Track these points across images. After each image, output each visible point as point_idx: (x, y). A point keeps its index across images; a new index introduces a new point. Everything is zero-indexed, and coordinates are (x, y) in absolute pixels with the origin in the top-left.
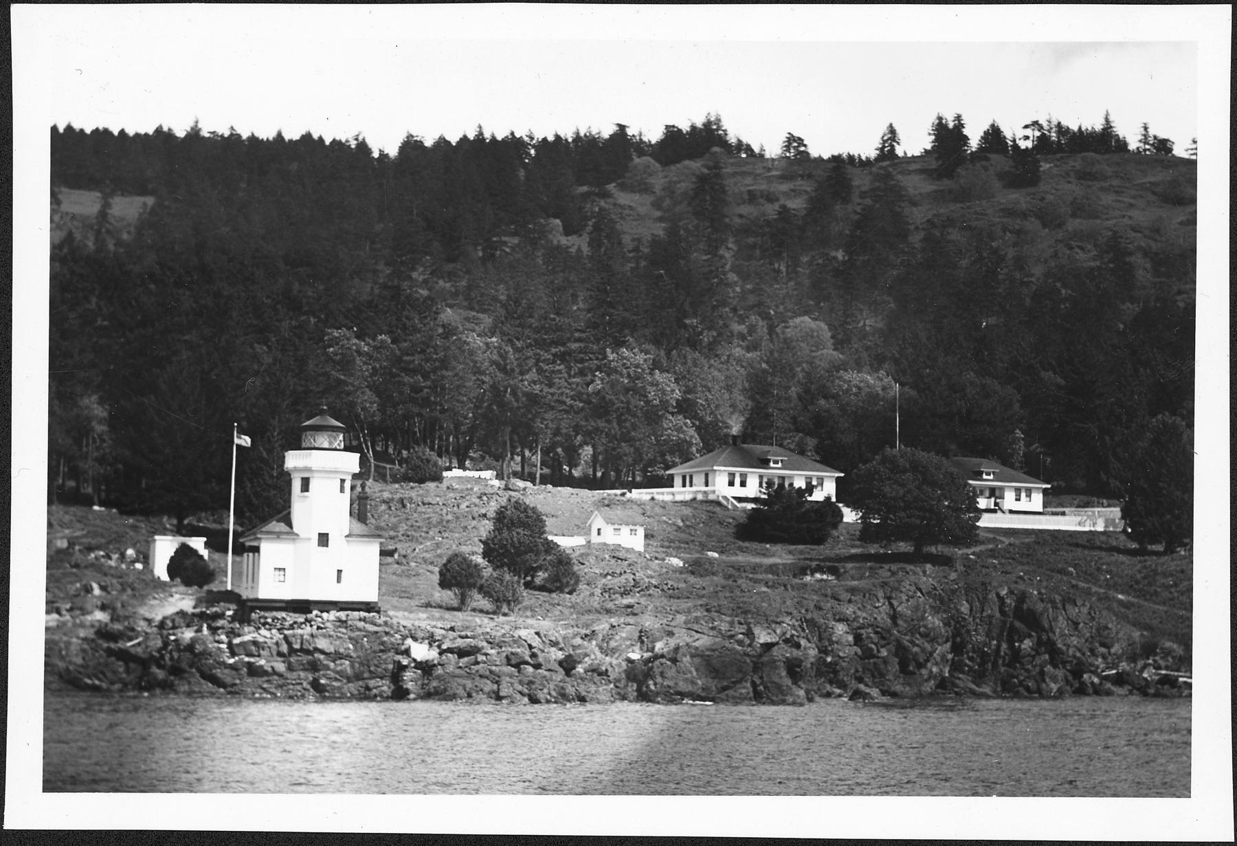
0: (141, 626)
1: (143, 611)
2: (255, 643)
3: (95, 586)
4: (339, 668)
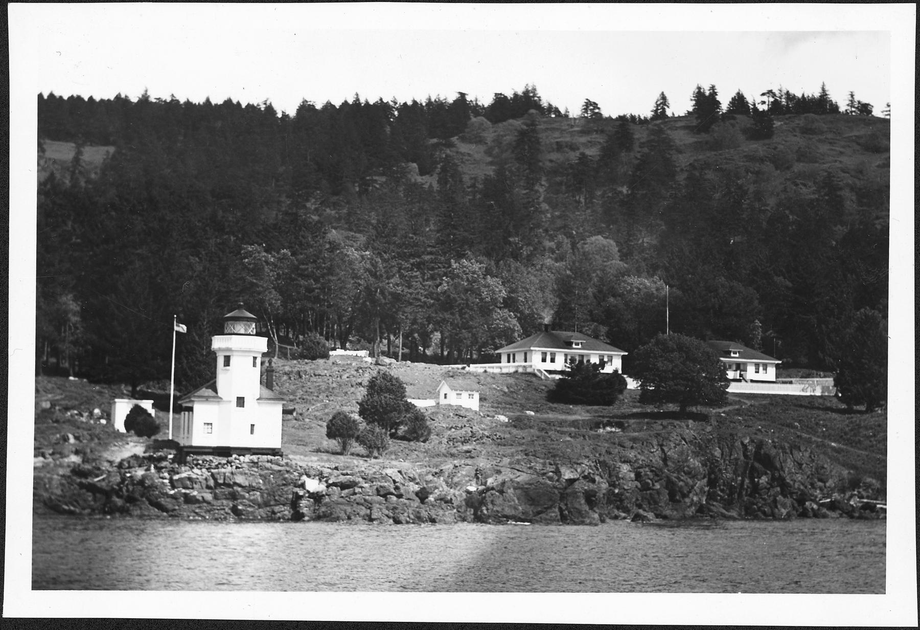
0: (105, 466)
1: (107, 455)
2: (190, 479)
3: (71, 436)
4: (252, 498)
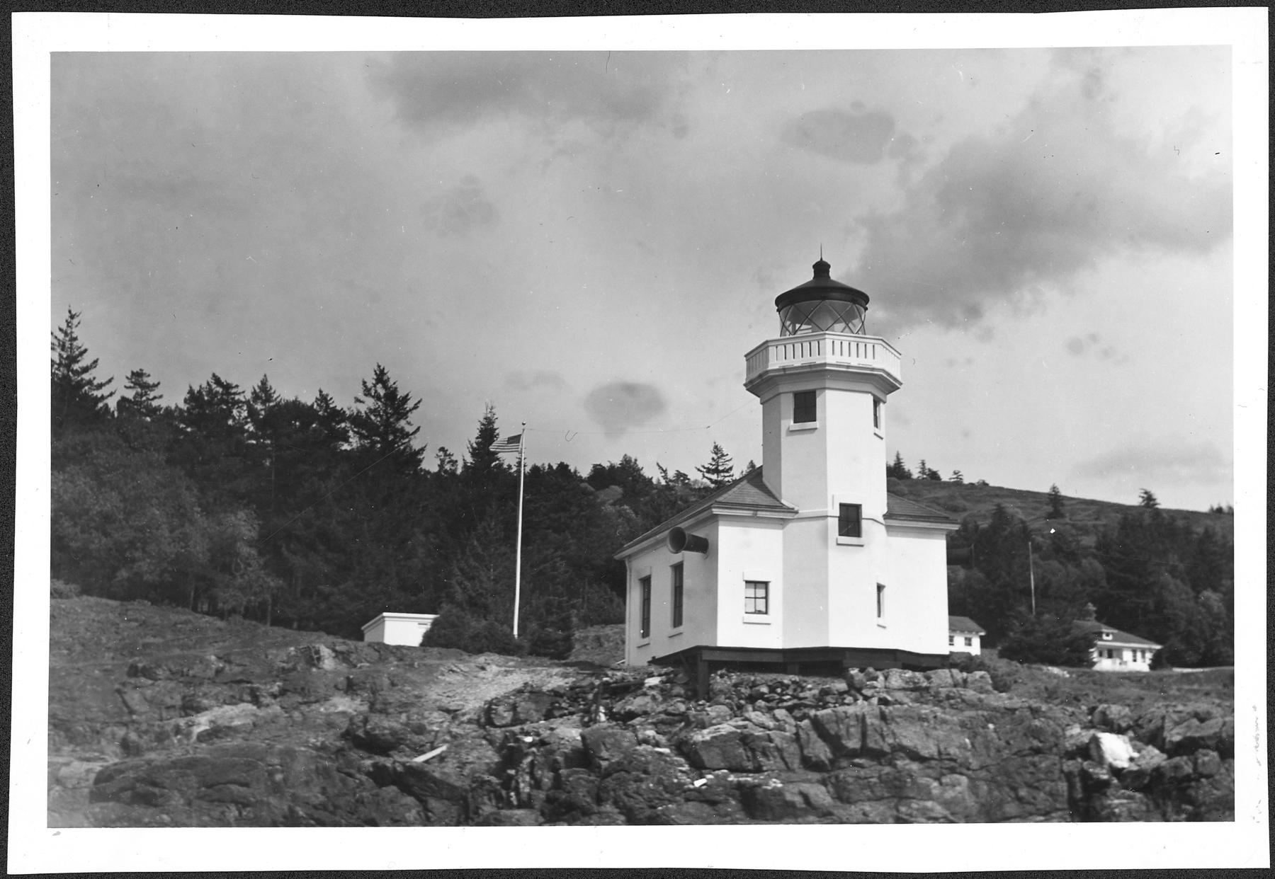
0: (436, 721)
1: (434, 693)
2: (745, 740)
3: (325, 651)
4: (950, 794)
